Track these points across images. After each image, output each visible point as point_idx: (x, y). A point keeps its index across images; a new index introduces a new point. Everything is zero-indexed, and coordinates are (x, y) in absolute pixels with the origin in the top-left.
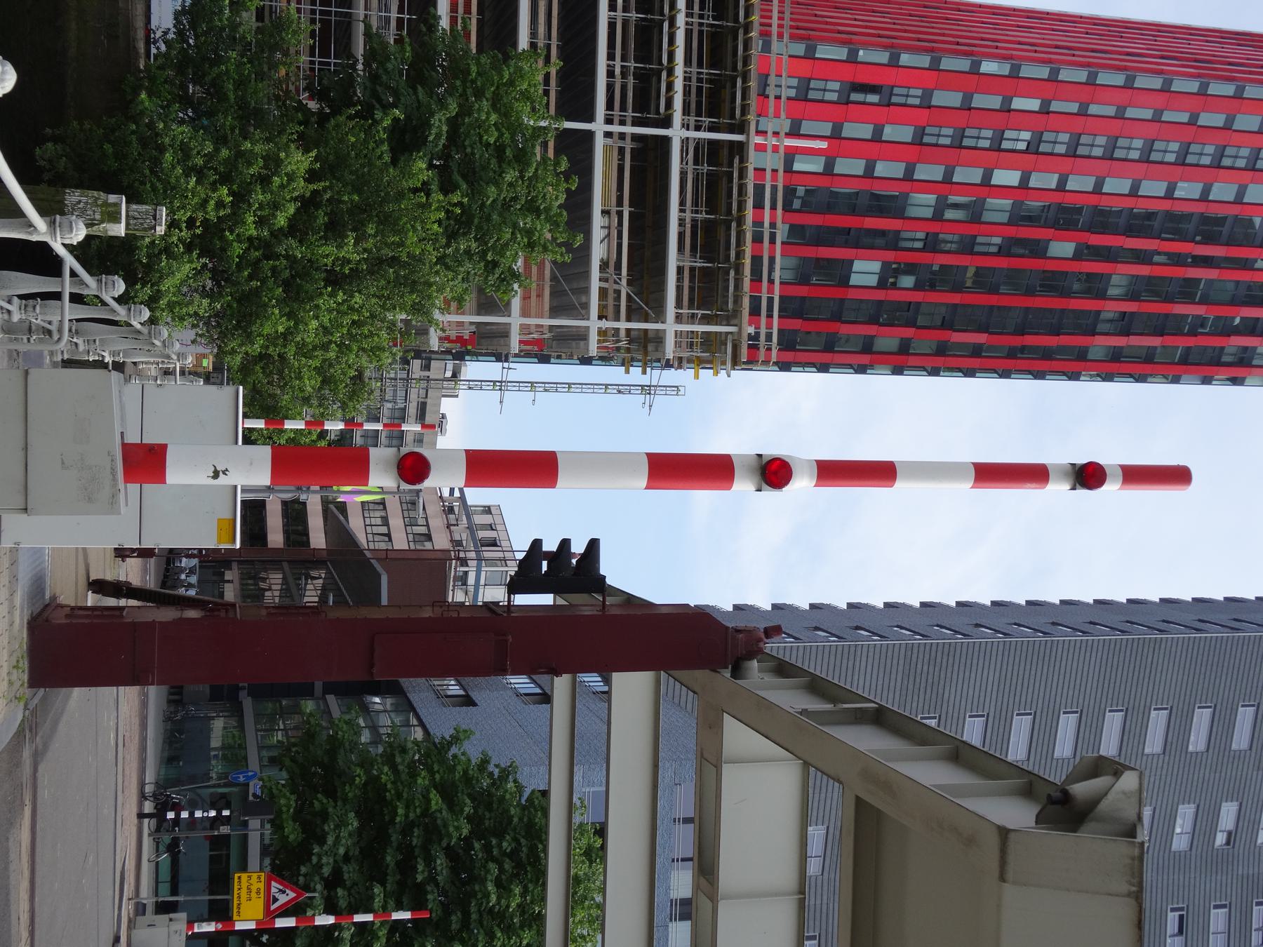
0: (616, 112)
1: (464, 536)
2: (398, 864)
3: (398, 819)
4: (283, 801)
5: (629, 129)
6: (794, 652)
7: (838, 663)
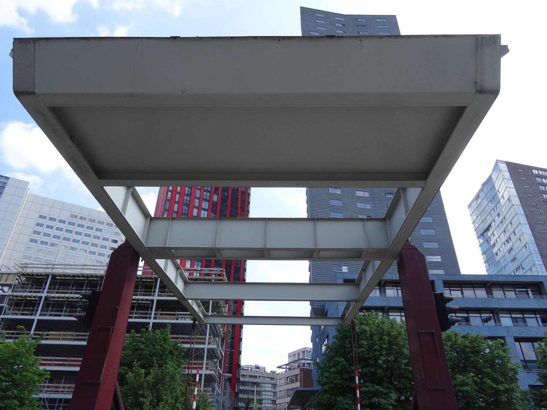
0: (148, 316)
1: (297, 364)
3: (340, 382)
5: (153, 312)
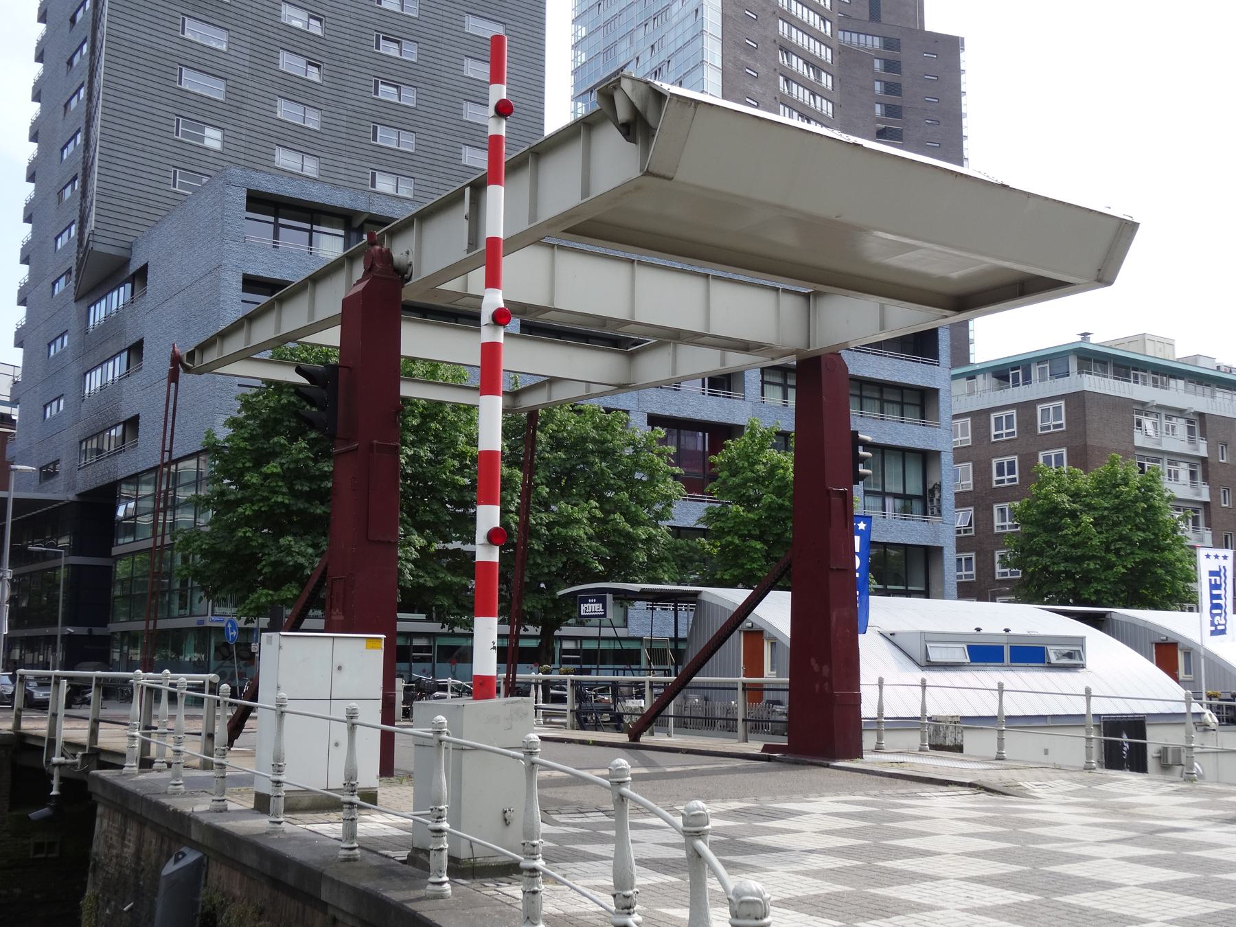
2: (322, 504)
3: (287, 501)
4: (263, 600)
6: (109, 98)
7: (125, 56)
